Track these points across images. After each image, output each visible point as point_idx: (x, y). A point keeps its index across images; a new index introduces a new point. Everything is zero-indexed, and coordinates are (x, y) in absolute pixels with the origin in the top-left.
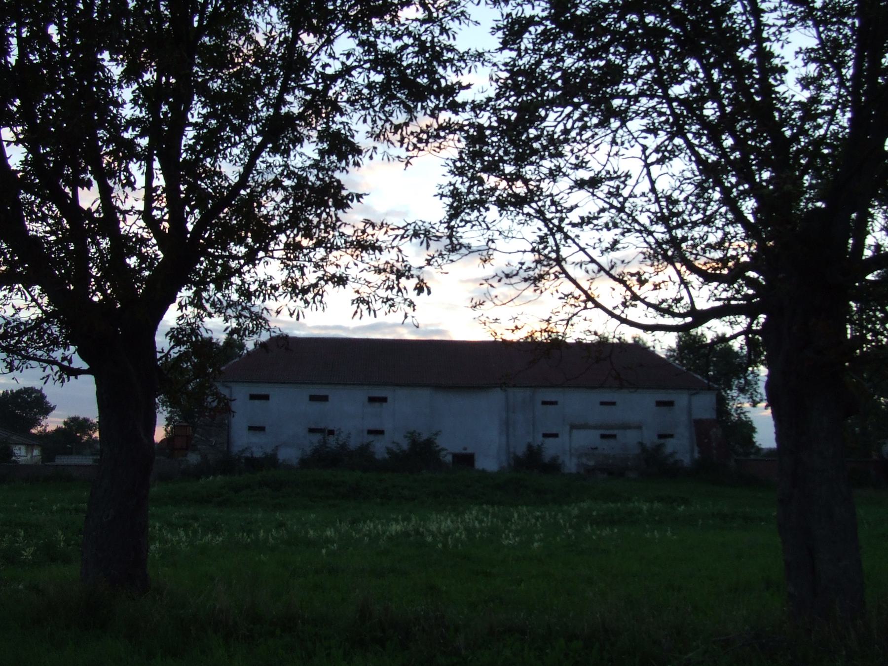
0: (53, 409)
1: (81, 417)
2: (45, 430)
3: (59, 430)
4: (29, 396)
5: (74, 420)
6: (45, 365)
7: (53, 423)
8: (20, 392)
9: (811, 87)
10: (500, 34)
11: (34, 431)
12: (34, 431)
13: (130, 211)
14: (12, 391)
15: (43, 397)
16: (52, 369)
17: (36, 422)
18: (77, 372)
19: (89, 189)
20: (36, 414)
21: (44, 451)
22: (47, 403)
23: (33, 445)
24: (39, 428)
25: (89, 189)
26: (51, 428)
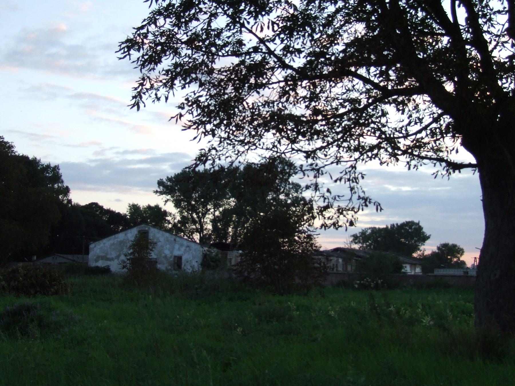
0: (428, 238)
1: (451, 243)
2: (423, 254)
3: (434, 254)
4: (410, 228)
5: (445, 246)
6: (435, 162)
7: (428, 248)
8: (404, 225)
9: (161, 187)
10: (462, 5)
11: (415, 255)
12: (415, 255)
13: (503, 11)
14: (397, 224)
15: (420, 228)
16: (441, 165)
17: (416, 248)
18: (457, 167)
19: (168, 177)
20: (415, 241)
21: (423, 270)
22: (423, 233)
23: (415, 264)
24: (419, 252)
25: (168, 177)
26: (428, 252)
